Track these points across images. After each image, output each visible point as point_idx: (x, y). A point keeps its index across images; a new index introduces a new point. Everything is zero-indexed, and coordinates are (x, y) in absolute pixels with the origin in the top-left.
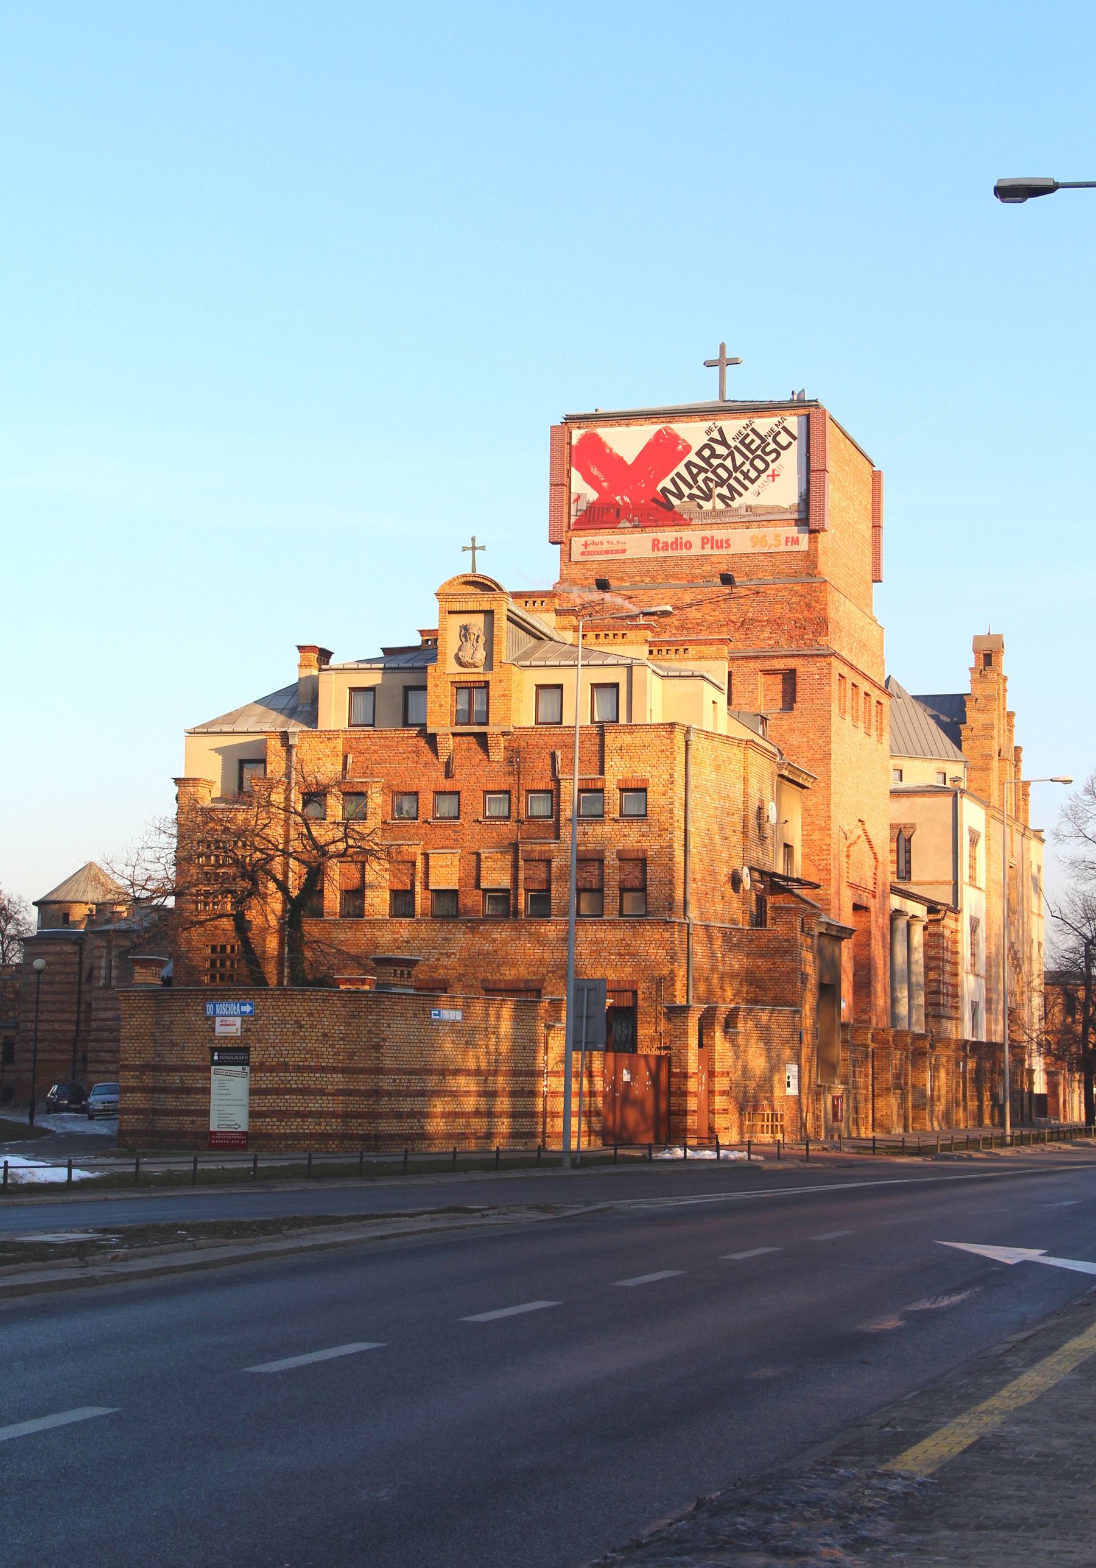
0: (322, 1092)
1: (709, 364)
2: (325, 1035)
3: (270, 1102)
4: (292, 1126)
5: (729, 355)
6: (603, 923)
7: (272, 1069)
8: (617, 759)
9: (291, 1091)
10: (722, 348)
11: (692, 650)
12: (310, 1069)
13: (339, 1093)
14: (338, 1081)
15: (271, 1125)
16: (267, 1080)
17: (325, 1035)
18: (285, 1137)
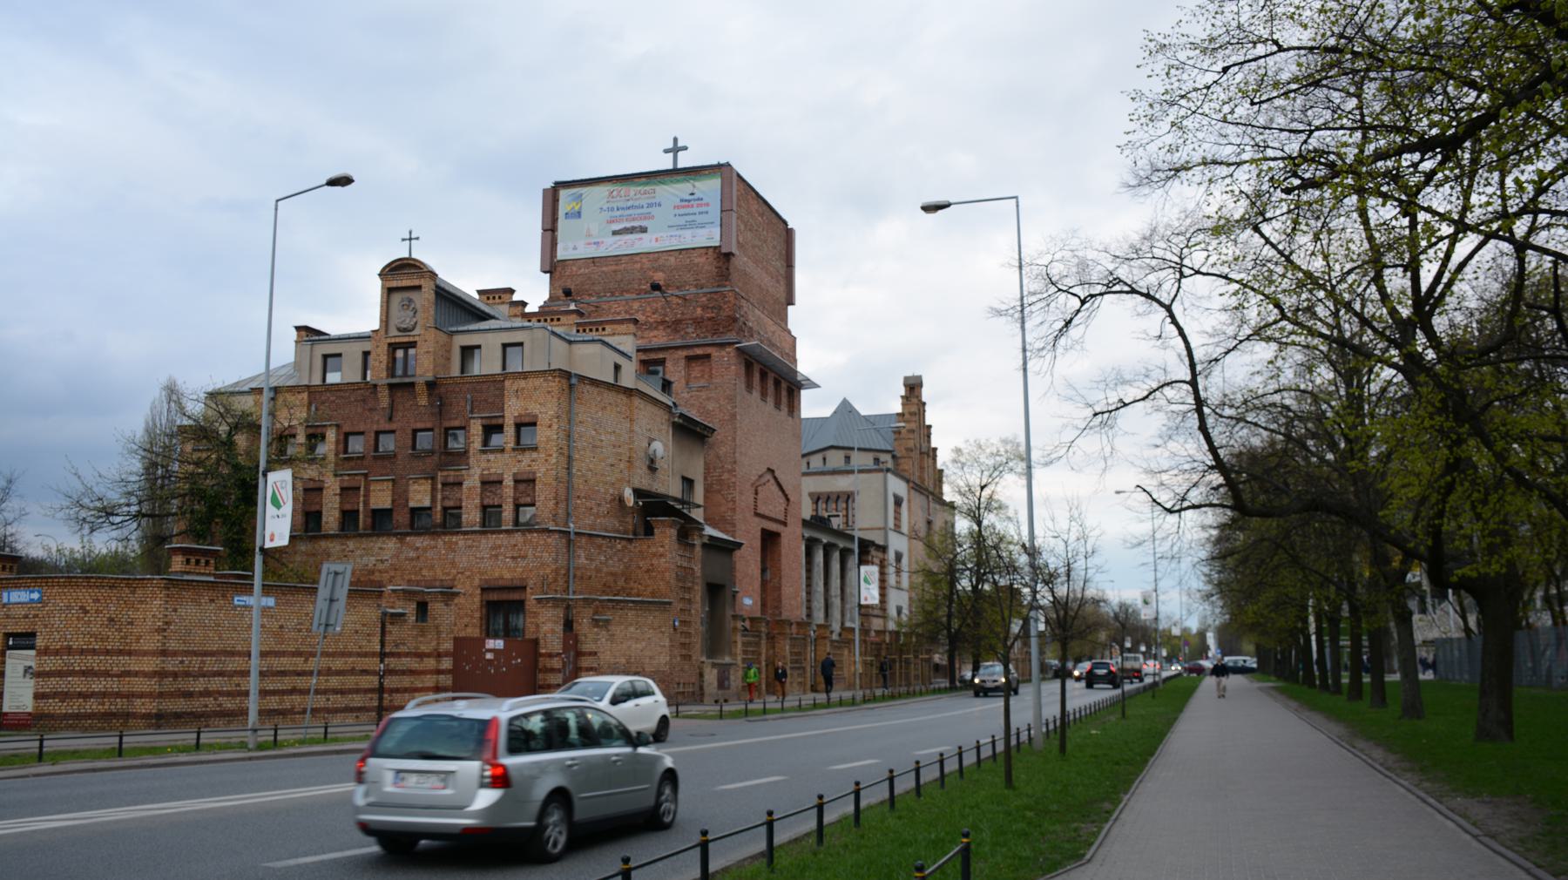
0: (107, 674)
1: (666, 151)
2: (111, 620)
3: (53, 684)
4: (75, 706)
5: (680, 144)
6: (501, 532)
7: (57, 653)
8: (514, 400)
9: (73, 673)
10: (675, 140)
11: (609, 329)
12: (94, 652)
13: (155, 674)
14: (149, 664)
15: (54, 706)
16: (52, 663)
17: (111, 620)
18: (66, 716)
